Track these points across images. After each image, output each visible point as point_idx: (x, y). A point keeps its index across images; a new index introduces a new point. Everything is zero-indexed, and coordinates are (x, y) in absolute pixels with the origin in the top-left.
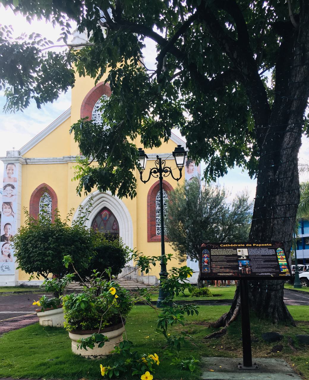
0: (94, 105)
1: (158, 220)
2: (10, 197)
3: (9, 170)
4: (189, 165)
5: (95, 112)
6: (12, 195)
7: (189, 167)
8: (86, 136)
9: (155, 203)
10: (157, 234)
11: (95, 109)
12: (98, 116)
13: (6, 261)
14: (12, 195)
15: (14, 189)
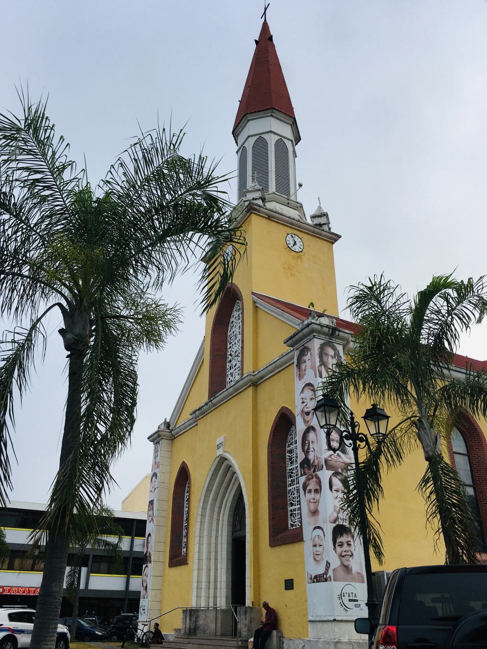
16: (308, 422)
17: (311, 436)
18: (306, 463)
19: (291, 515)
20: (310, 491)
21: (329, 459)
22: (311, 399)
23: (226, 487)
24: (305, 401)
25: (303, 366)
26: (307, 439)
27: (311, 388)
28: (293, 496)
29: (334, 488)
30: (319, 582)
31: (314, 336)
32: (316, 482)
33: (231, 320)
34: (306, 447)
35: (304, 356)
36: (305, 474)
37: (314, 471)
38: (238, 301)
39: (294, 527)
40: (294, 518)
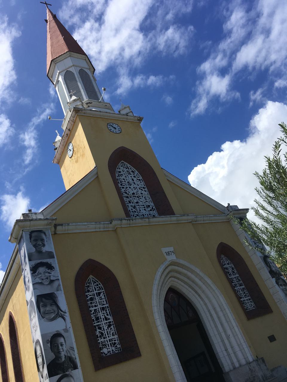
12: (123, 180)
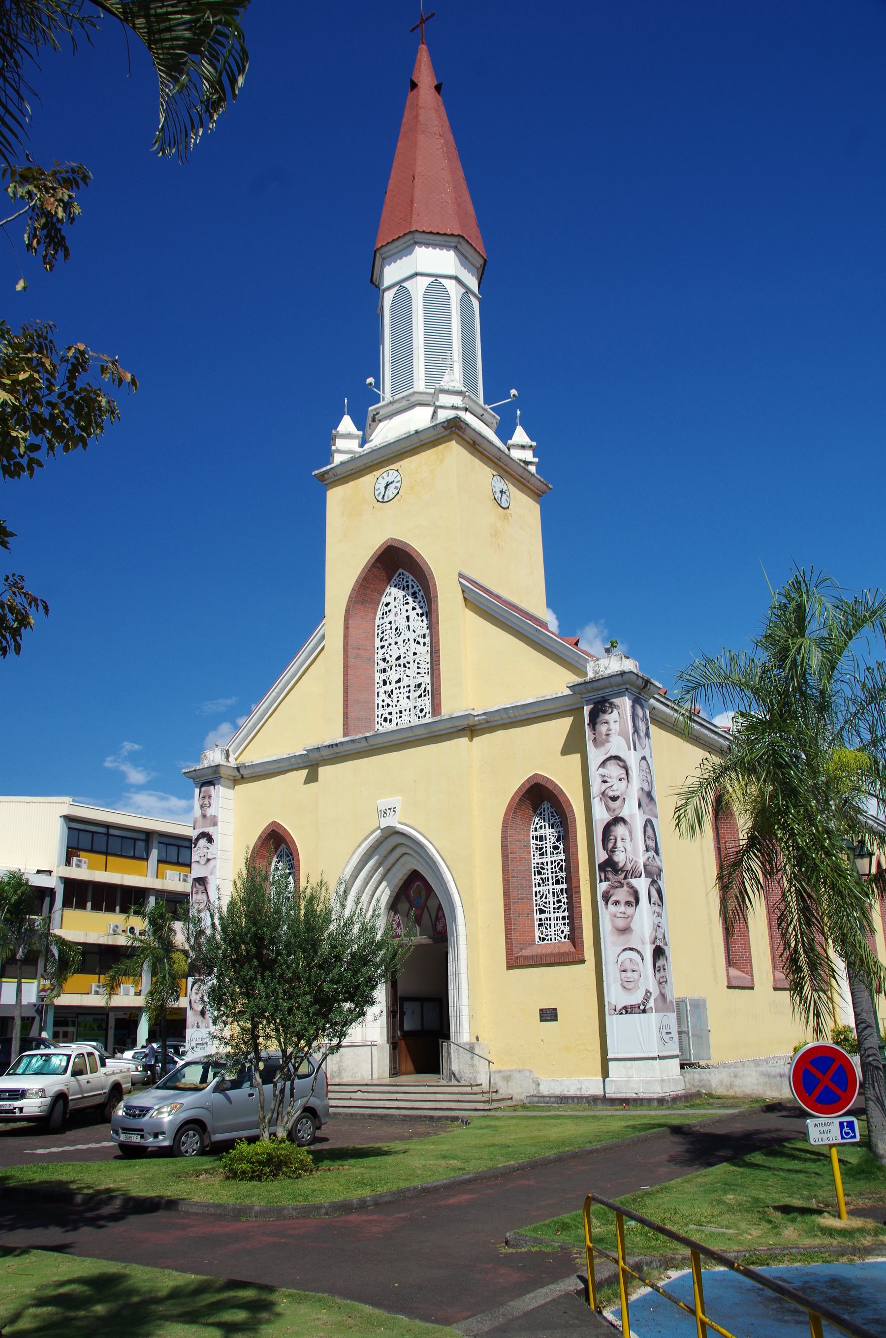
0: (380, 602)
1: (539, 896)
2: (205, 864)
3: (204, 798)
4: (598, 720)
5: (383, 618)
6: (208, 860)
7: (597, 726)
8: (155, 45)
9: (528, 846)
10: (537, 939)
11: (382, 612)
12: (389, 626)
13: (198, 1027)
14: (208, 860)
15: (211, 843)
16: (614, 810)
17: (620, 830)
18: (610, 866)
19: (540, 925)
20: (616, 903)
21: (648, 863)
22: (620, 780)
23: (365, 879)
24: (608, 780)
25: (603, 729)
26: (613, 834)
27: (621, 764)
28: (545, 901)
29: (653, 900)
30: (631, 1013)
31: (627, 689)
32: (628, 891)
33: (385, 600)
34: (610, 845)
35: (604, 712)
36: (607, 879)
37: (625, 878)
38: (401, 571)
39: (545, 942)
40: (547, 929)
